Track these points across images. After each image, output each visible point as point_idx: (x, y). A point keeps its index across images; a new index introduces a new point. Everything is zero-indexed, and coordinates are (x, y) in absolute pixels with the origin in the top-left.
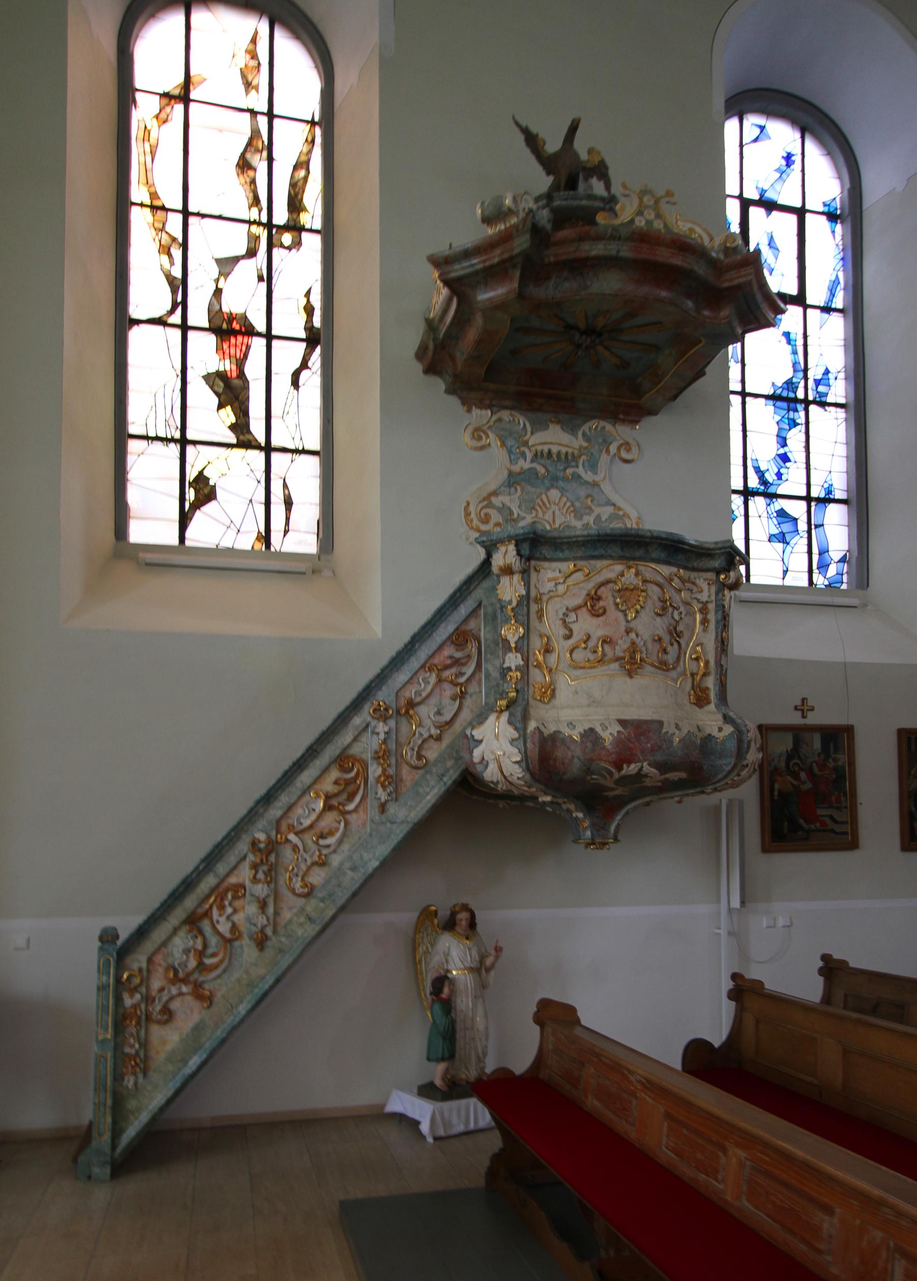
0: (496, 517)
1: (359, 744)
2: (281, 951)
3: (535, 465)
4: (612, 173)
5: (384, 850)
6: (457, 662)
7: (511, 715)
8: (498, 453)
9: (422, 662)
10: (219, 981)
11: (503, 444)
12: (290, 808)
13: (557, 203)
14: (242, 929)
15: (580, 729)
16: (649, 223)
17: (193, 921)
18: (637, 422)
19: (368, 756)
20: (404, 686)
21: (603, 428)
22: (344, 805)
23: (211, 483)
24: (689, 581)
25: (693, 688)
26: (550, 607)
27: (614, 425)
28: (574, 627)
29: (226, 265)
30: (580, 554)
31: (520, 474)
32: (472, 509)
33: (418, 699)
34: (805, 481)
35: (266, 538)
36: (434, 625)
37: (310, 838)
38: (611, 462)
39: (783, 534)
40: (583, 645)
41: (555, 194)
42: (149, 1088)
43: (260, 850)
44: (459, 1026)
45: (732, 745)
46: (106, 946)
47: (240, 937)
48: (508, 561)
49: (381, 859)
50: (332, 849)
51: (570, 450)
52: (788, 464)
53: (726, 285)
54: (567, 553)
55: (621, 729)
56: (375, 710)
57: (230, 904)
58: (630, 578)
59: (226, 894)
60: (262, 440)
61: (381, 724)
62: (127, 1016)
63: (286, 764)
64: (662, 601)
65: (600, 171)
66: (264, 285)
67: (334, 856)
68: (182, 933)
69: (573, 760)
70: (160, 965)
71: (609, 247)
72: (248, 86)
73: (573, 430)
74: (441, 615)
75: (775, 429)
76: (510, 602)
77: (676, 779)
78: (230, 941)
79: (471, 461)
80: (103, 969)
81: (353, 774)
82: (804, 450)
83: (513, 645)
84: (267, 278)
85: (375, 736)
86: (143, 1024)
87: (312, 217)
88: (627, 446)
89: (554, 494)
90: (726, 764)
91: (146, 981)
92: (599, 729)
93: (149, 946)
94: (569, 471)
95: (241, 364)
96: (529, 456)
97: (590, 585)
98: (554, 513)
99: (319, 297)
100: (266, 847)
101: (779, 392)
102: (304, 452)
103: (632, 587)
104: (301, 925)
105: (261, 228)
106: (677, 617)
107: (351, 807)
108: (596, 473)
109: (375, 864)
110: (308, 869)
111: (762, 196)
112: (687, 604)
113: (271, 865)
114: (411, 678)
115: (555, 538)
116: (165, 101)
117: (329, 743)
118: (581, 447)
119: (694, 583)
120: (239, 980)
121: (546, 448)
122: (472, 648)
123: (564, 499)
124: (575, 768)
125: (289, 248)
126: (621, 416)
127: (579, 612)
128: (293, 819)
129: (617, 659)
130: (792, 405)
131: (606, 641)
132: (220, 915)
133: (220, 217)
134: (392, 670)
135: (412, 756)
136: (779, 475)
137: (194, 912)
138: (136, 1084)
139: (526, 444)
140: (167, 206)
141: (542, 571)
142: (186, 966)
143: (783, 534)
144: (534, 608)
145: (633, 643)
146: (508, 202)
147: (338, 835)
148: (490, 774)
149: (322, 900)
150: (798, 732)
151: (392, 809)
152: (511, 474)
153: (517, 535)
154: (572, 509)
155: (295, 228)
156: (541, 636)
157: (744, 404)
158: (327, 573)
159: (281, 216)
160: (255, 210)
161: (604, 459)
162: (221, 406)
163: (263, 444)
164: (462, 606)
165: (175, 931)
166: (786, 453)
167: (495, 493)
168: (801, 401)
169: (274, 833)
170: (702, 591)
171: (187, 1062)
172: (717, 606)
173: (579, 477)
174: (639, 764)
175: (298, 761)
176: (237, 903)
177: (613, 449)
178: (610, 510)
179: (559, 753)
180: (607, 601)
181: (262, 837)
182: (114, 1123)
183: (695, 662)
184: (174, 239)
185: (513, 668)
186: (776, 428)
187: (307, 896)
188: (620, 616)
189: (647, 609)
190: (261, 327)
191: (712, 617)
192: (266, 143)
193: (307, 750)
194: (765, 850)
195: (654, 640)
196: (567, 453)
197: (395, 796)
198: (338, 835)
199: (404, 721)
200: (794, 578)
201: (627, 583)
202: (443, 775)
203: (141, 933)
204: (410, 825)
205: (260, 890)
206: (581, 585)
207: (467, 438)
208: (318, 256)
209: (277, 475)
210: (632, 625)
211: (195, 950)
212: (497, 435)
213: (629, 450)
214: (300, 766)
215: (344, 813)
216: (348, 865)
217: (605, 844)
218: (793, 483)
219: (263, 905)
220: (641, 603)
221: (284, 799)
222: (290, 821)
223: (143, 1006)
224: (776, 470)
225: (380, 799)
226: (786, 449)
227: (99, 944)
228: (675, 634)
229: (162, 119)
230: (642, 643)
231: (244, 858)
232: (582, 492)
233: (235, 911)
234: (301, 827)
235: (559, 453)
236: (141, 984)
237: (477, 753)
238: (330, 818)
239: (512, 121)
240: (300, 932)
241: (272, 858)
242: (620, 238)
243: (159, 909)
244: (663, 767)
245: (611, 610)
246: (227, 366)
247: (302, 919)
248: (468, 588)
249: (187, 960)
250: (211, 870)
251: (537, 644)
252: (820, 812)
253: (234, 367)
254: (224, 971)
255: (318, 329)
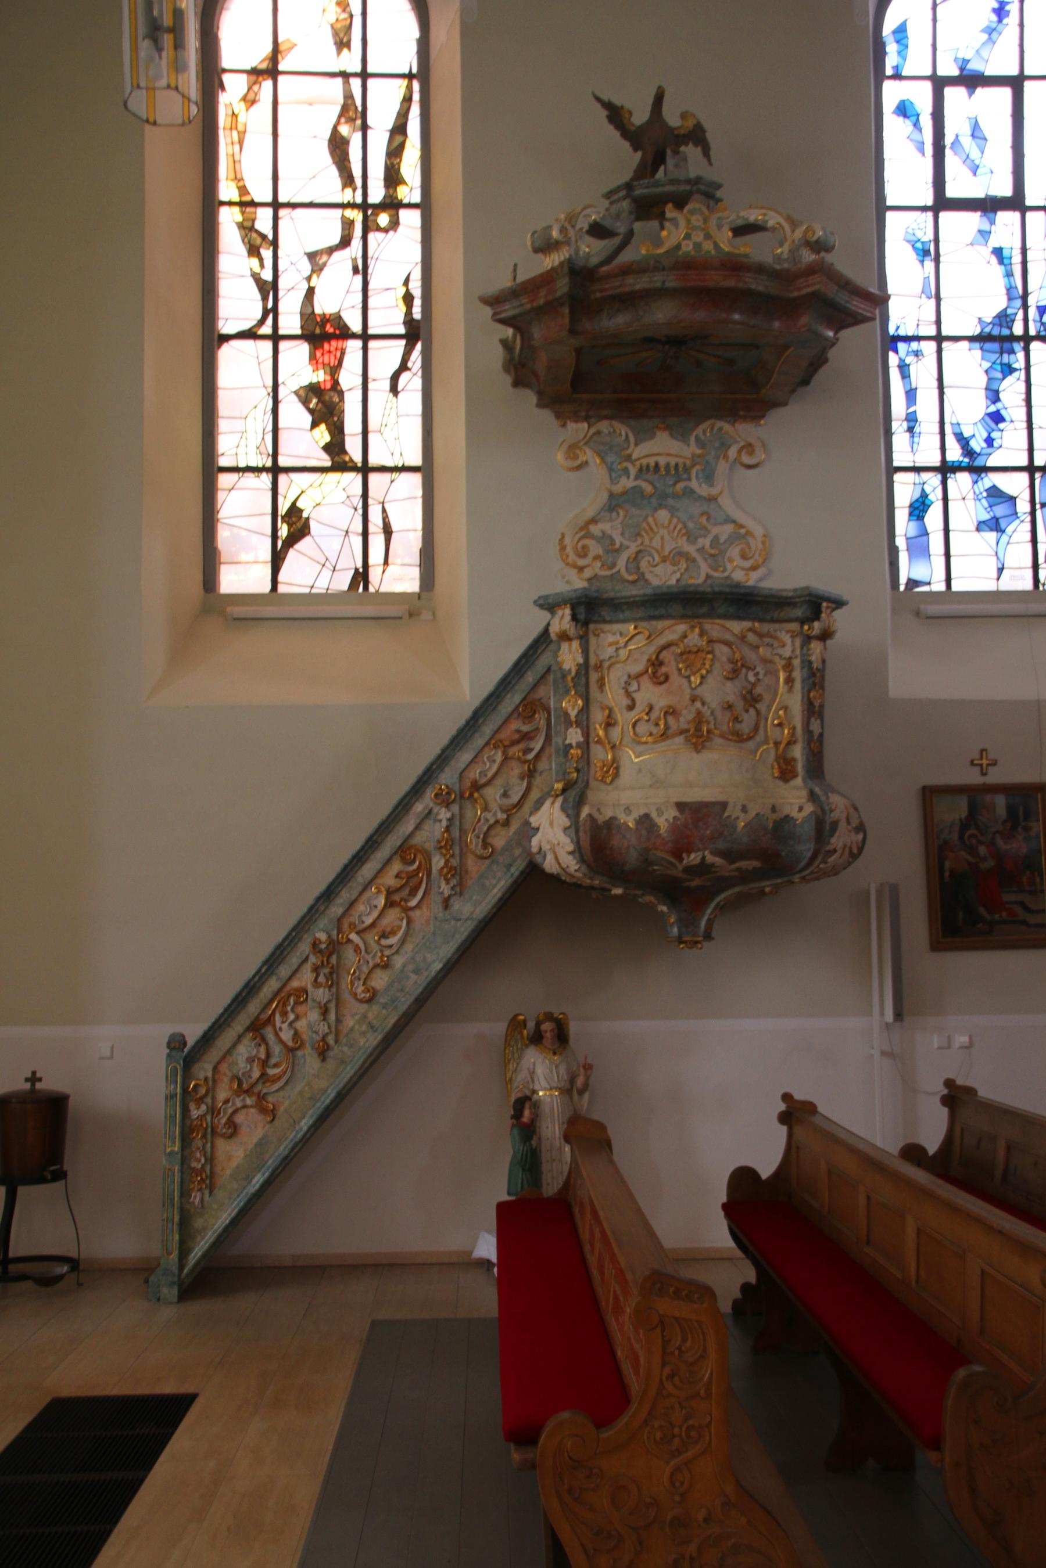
0: (595, 549)
1: (422, 832)
2: (343, 1062)
3: (639, 482)
4: (709, 136)
5: (448, 950)
6: (526, 737)
7: (565, 801)
8: (597, 470)
9: (487, 738)
10: (281, 1094)
11: (603, 460)
12: (352, 904)
13: (638, 192)
14: (305, 1037)
15: (635, 814)
16: (697, 246)
17: (256, 1027)
18: (763, 417)
19: (430, 846)
20: (468, 766)
21: (721, 429)
22: (406, 901)
23: (305, 515)
24: (768, 635)
25: (777, 759)
26: (612, 676)
27: (733, 425)
28: (637, 696)
29: (316, 260)
30: (640, 615)
31: (623, 494)
32: (568, 541)
33: (483, 780)
34: (1025, 446)
35: (362, 576)
36: (498, 697)
37: (372, 937)
38: (731, 469)
39: (996, 520)
40: (646, 718)
41: (635, 183)
42: (215, 1206)
43: (321, 951)
44: (545, 1156)
45: (809, 830)
46: (174, 1053)
47: (301, 1046)
48: (563, 628)
49: (445, 960)
50: (394, 949)
51: (680, 461)
52: (1001, 426)
53: (796, 294)
54: (627, 614)
55: (677, 814)
56: (436, 795)
57: (292, 1010)
58: (694, 639)
59: (288, 999)
60: (358, 458)
61: (443, 810)
62: (195, 1128)
63: (344, 858)
64: (732, 663)
65: (697, 136)
66: (359, 278)
67: (396, 957)
68: (246, 1041)
69: (628, 848)
70: (225, 1075)
71: (655, 279)
72: (342, 44)
73: (683, 437)
74: (505, 684)
75: (983, 380)
76: (570, 670)
77: (750, 868)
78: (292, 1050)
79: (565, 484)
80: (171, 1078)
81: (415, 866)
82: (1024, 404)
83: (573, 719)
84: (362, 269)
85: (438, 824)
86: (209, 1137)
87: (410, 191)
88: (749, 448)
89: (663, 515)
90: (806, 849)
91: (211, 1091)
92: (654, 815)
93: (214, 1054)
94: (680, 486)
95: (334, 370)
96: (633, 471)
97: (652, 649)
98: (662, 538)
99: (419, 284)
100: (327, 947)
101: (987, 330)
102: (405, 469)
103: (695, 649)
104: (363, 1033)
105: (356, 211)
106: (751, 678)
107: (413, 903)
108: (712, 485)
109: (438, 966)
110: (371, 972)
111: (962, 69)
112: (765, 661)
113: (332, 967)
114: (476, 757)
115: (612, 599)
116: (253, 78)
117: (390, 832)
118: (693, 455)
119: (775, 638)
120: (301, 1093)
121: (652, 461)
122: (540, 719)
123: (675, 520)
124: (632, 859)
125: (386, 231)
126: (742, 413)
127: (641, 679)
128: (354, 918)
129: (682, 732)
130: (1006, 345)
131: (671, 712)
132: (283, 1022)
133: (311, 205)
134: (454, 750)
135: (477, 845)
136: (989, 441)
137: (257, 1018)
138: (202, 1200)
139: (628, 458)
140: (257, 200)
141: (602, 635)
142: (250, 1077)
143: (996, 520)
144: (594, 677)
145: (699, 713)
146: (555, 234)
147: (400, 934)
148: (549, 865)
149: (385, 1006)
150: (974, 794)
151: (456, 905)
152: (612, 495)
153: (571, 599)
154: (684, 531)
155: (391, 205)
156: (603, 709)
157: (939, 351)
158: (426, 616)
159: (377, 194)
160: (349, 191)
161: (722, 467)
162: (314, 425)
163: (360, 465)
164: (529, 673)
165: (240, 1038)
166: (998, 411)
167: (594, 521)
168: (1018, 339)
169: (335, 932)
170: (784, 646)
171: (251, 1181)
172: (802, 662)
173: (692, 492)
174: (700, 854)
175: (358, 853)
176: (300, 1009)
177: (732, 453)
178: (729, 528)
179: (616, 842)
180: (671, 666)
181: (322, 936)
182: (182, 1242)
183: (778, 729)
184: (264, 237)
185: (574, 744)
186: (985, 378)
187: (369, 1001)
188: (684, 681)
189: (715, 672)
190: (356, 327)
191: (797, 675)
192: (360, 109)
193: (367, 842)
194: (936, 946)
195: (724, 709)
196: (677, 465)
197: (460, 889)
198: (400, 934)
199: (468, 805)
200: (1012, 578)
201: (691, 644)
202: (511, 865)
203: (207, 1039)
204: (475, 923)
205: (321, 994)
206: (643, 649)
207: (560, 457)
208: (417, 235)
209: (374, 499)
210: (696, 692)
211: (259, 1059)
212: (595, 452)
213: (751, 453)
214: (360, 859)
215: (407, 910)
216: (410, 967)
217: (697, 942)
218: (1011, 449)
219: (325, 1012)
220: (707, 666)
221: (346, 895)
222: (352, 919)
223: (209, 1118)
224: (985, 435)
225: (442, 893)
226: (999, 405)
227: (168, 1051)
228: (751, 699)
229: (250, 101)
230: (709, 712)
231: (307, 959)
232: (696, 509)
233: (297, 1018)
234: (362, 927)
235: (668, 465)
236: (206, 1095)
237: (535, 842)
238: (393, 916)
239: (593, 99)
240: (362, 1041)
241: (334, 960)
242: (664, 269)
243: (222, 1014)
244: (730, 856)
245: (675, 678)
246: (320, 376)
247: (364, 1028)
248: (535, 652)
249: (251, 1070)
250: (272, 973)
251: (598, 716)
252: (1006, 897)
253: (328, 378)
254: (287, 1083)
255: (418, 321)
